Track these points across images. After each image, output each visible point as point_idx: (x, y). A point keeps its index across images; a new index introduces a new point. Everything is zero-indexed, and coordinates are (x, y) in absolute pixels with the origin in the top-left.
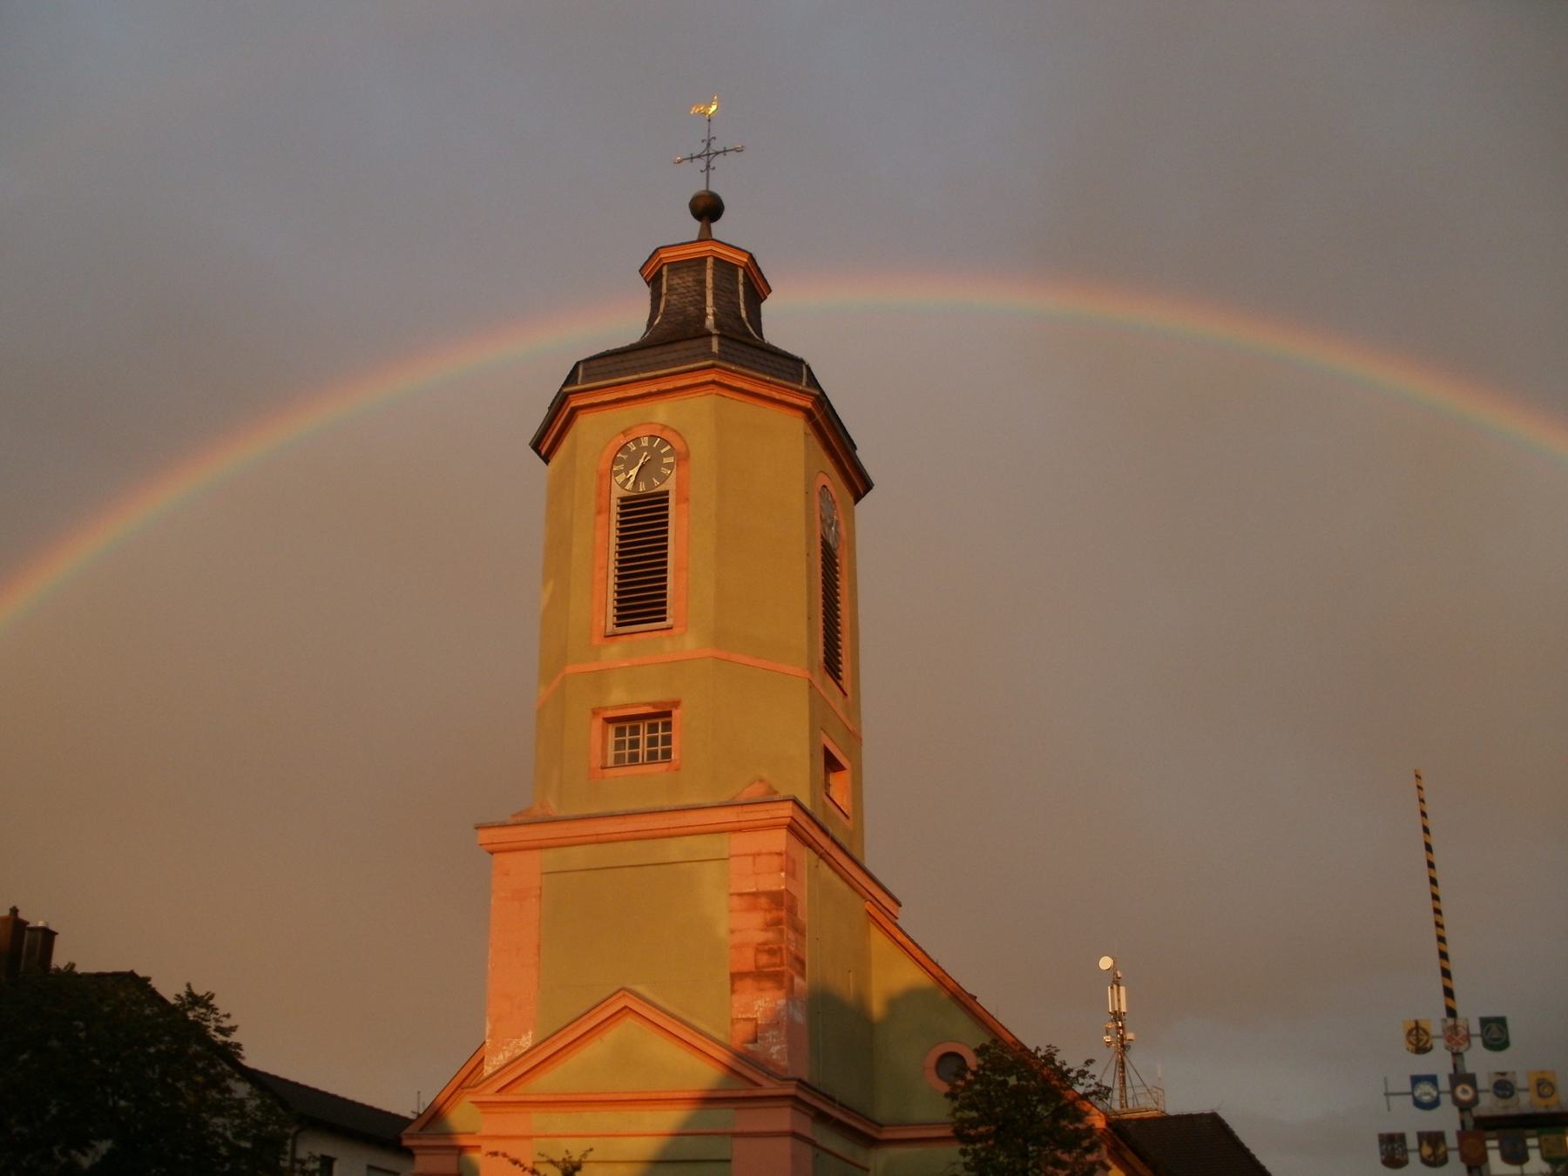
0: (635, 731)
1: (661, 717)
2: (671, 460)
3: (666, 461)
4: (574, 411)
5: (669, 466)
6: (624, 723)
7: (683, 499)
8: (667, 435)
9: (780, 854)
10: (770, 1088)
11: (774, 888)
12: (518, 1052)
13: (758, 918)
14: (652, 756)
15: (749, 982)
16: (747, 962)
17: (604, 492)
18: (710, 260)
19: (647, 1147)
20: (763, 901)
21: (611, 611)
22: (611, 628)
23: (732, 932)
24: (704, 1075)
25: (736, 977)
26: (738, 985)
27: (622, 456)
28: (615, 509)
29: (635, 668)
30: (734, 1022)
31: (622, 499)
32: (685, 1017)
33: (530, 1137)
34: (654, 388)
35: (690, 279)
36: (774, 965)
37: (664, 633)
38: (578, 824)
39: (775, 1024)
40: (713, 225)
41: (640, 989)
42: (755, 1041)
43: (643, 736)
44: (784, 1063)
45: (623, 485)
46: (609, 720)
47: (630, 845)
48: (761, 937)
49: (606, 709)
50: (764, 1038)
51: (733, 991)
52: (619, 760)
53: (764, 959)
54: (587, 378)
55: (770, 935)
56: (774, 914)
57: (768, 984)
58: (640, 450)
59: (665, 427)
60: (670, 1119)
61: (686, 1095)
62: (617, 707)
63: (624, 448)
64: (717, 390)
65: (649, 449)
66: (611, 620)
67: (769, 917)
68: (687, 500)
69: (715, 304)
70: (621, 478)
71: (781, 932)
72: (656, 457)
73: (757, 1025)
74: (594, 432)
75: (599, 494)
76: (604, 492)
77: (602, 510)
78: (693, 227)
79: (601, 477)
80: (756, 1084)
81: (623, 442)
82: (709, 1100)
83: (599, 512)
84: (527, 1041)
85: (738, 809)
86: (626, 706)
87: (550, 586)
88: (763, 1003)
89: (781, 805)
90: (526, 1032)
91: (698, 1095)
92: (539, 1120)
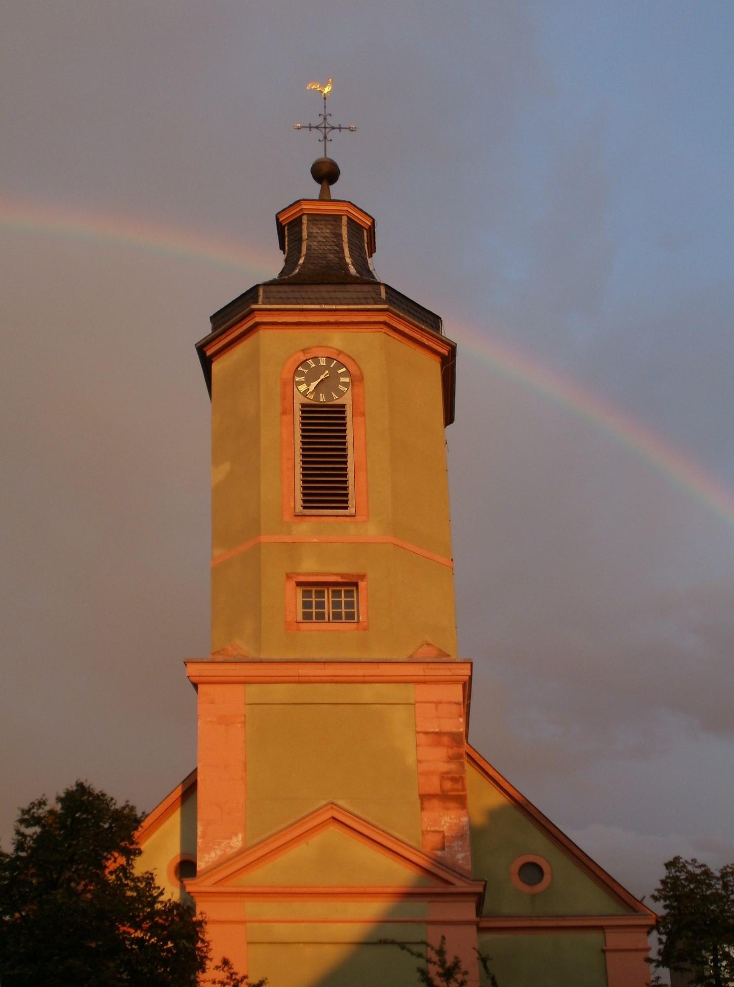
0: (320, 594)
1: (351, 585)
2: (347, 380)
3: (343, 380)
4: (257, 325)
5: (345, 384)
6: (311, 587)
7: (359, 413)
8: (342, 359)
9: (458, 704)
10: (461, 886)
11: (454, 730)
12: (230, 852)
13: (441, 753)
14: (337, 616)
15: (435, 803)
16: (434, 785)
17: (287, 396)
18: (345, 219)
19: (353, 932)
20: (446, 739)
21: (299, 496)
22: (299, 509)
23: (419, 762)
24: (403, 875)
25: (425, 798)
26: (426, 804)
27: (303, 367)
28: (298, 413)
29: (322, 544)
30: (424, 833)
31: (303, 405)
32: (386, 829)
33: (243, 922)
34: (332, 319)
35: (327, 231)
36: (457, 790)
37: (347, 519)
38: (284, 666)
39: (461, 837)
40: (332, 187)
41: (341, 803)
42: (443, 849)
43: (328, 598)
44: (469, 867)
45: (304, 394)
46: (299, 584)
47: (328, 687)
48: (445, 767)
49: (299, 574)
50: (451, 847)
51: (422, 809)
52: (307, 616)
53: (448, 785)
54: (267, 300)
55: (452, 766)
56: (455, 750)
57: (452, 805)
58: (319, 370)
59: (340, 352)
60: (374, 909)
61: (390, 890)
62: (309, 574)
63: (303, 363)
64: (386, 329)
65: (327, 367)
66: (299, 503)
67: (451, 752)
68: (363, 414)
69: (351, 256)
70: (303, 388)
71: (462, 765)
72: (334, 377)
73: (444, 837)
74: (276, 347)
75: (284, 398)
76: (287, 396)
77: (286, 411)
78: (314, 189)
79: (284, 384)
80: (451, 884)
81: (303, 358)
82: (408, 895)
83: (284, 413)
84: (237, 842)
85: (426, 666)
86: (317, 574)
87: (226, 467)
88: (449, 820)
89: (462, 666)
90: (236, 834)
91: (404, 890)
92: (252, 908)
